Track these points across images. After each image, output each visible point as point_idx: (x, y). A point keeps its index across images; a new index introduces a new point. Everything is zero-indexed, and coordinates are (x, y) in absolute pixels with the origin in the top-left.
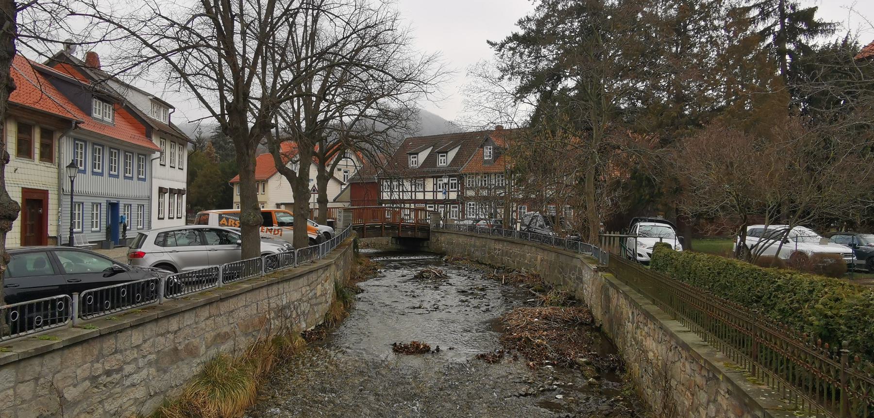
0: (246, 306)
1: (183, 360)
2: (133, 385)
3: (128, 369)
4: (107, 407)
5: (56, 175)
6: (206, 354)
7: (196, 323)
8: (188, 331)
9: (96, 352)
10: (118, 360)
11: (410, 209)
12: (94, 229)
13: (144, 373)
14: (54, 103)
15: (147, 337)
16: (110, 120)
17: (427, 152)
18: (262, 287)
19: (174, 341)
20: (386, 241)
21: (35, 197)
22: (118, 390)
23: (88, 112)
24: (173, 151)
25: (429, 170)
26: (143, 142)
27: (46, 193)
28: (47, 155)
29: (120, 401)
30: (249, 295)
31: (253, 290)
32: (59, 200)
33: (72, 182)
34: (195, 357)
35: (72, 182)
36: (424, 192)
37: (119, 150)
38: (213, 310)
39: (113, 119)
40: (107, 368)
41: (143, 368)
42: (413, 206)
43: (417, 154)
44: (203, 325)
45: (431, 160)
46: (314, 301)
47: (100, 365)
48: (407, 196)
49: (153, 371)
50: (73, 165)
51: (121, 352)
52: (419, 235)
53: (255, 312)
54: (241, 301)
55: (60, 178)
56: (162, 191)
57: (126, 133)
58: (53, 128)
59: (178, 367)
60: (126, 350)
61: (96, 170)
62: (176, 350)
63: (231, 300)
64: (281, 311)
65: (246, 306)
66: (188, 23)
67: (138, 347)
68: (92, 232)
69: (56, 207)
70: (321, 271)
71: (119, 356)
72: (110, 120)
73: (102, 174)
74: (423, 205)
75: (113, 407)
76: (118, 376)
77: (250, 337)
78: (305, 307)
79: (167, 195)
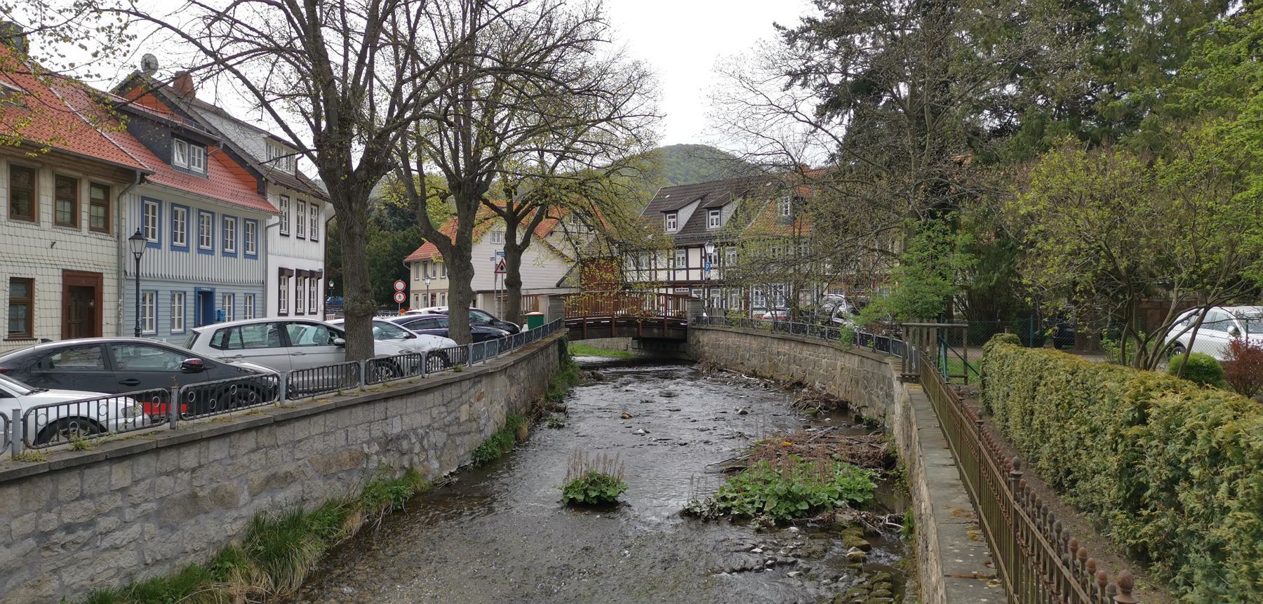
0: (325, 434)
1: (206, 513)
2: (115, 548)
3: (104, 523)
4: (67, 578)
5: (115, 251)
6: (247, 508)
7: (232, 457)
8: (216, 468)
9: (45, 496)
10: (86, 509)
11: (666, 295)
12: (176, 330)
13: (135, 530)
14: (116, 147)
15: (139, 476)
16: (201, 170)
17: (691, 209)
18: (354, 406)
19: (190, 483)
20: (622, 346)
21: (84, 283)
22: (86, 553)
23: (167, 159)
24: (301, 214)
25: (692, 238)
26: (250, 202)
27: (98, 277)
28: (103, 226)
29: (90, 571)
30: (331, 418)
31: (337, 409)
32: (119, 286)
33: (138, 260)
34: (228, 508)
35: (138, 260)
36: (688, 269)
37: (188, 208)
38: (264, 438)
39: (206, 169)
40: (66, 520)
41: (133, 522)
42: (670, 291)
43: (676, 211)
44: (245, 460)
45: (696, 221)
46: (454, 429)
47: (53, 516)
48: (662, 276)
49: (151, 527)
50: (138, 236)
51: (92, 497)
52: (671, 333)
53: (343, 443)
54: (318, 425)
55: (120, 255)
56: (283, 272)
57: (225, 189)
58: (109, 182)
59: (197, 522)
60: (100, 494)
61: (204, 247)
62: (194, 497)
63: (297, 424)
64: (389, 443)
65: (325, 434)
66: (228, 9)
67: (123, 490)
68: (172, 334)
69: (114, 297)
70: (466, 385)
71: (87, 503)
72: (201, 170)
73: (186, 249)
74: (686, 290)
75: (77, 579)
76: (87, 534)
77: (333, 481)
78: (438, 438)
79: (292, 280)
